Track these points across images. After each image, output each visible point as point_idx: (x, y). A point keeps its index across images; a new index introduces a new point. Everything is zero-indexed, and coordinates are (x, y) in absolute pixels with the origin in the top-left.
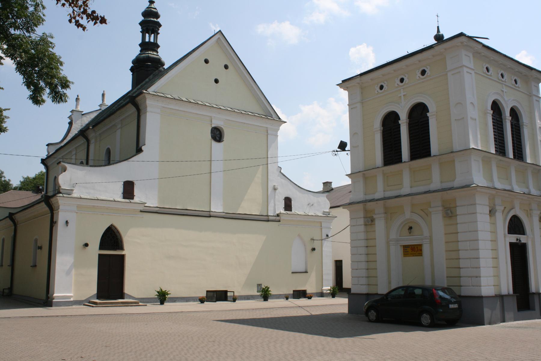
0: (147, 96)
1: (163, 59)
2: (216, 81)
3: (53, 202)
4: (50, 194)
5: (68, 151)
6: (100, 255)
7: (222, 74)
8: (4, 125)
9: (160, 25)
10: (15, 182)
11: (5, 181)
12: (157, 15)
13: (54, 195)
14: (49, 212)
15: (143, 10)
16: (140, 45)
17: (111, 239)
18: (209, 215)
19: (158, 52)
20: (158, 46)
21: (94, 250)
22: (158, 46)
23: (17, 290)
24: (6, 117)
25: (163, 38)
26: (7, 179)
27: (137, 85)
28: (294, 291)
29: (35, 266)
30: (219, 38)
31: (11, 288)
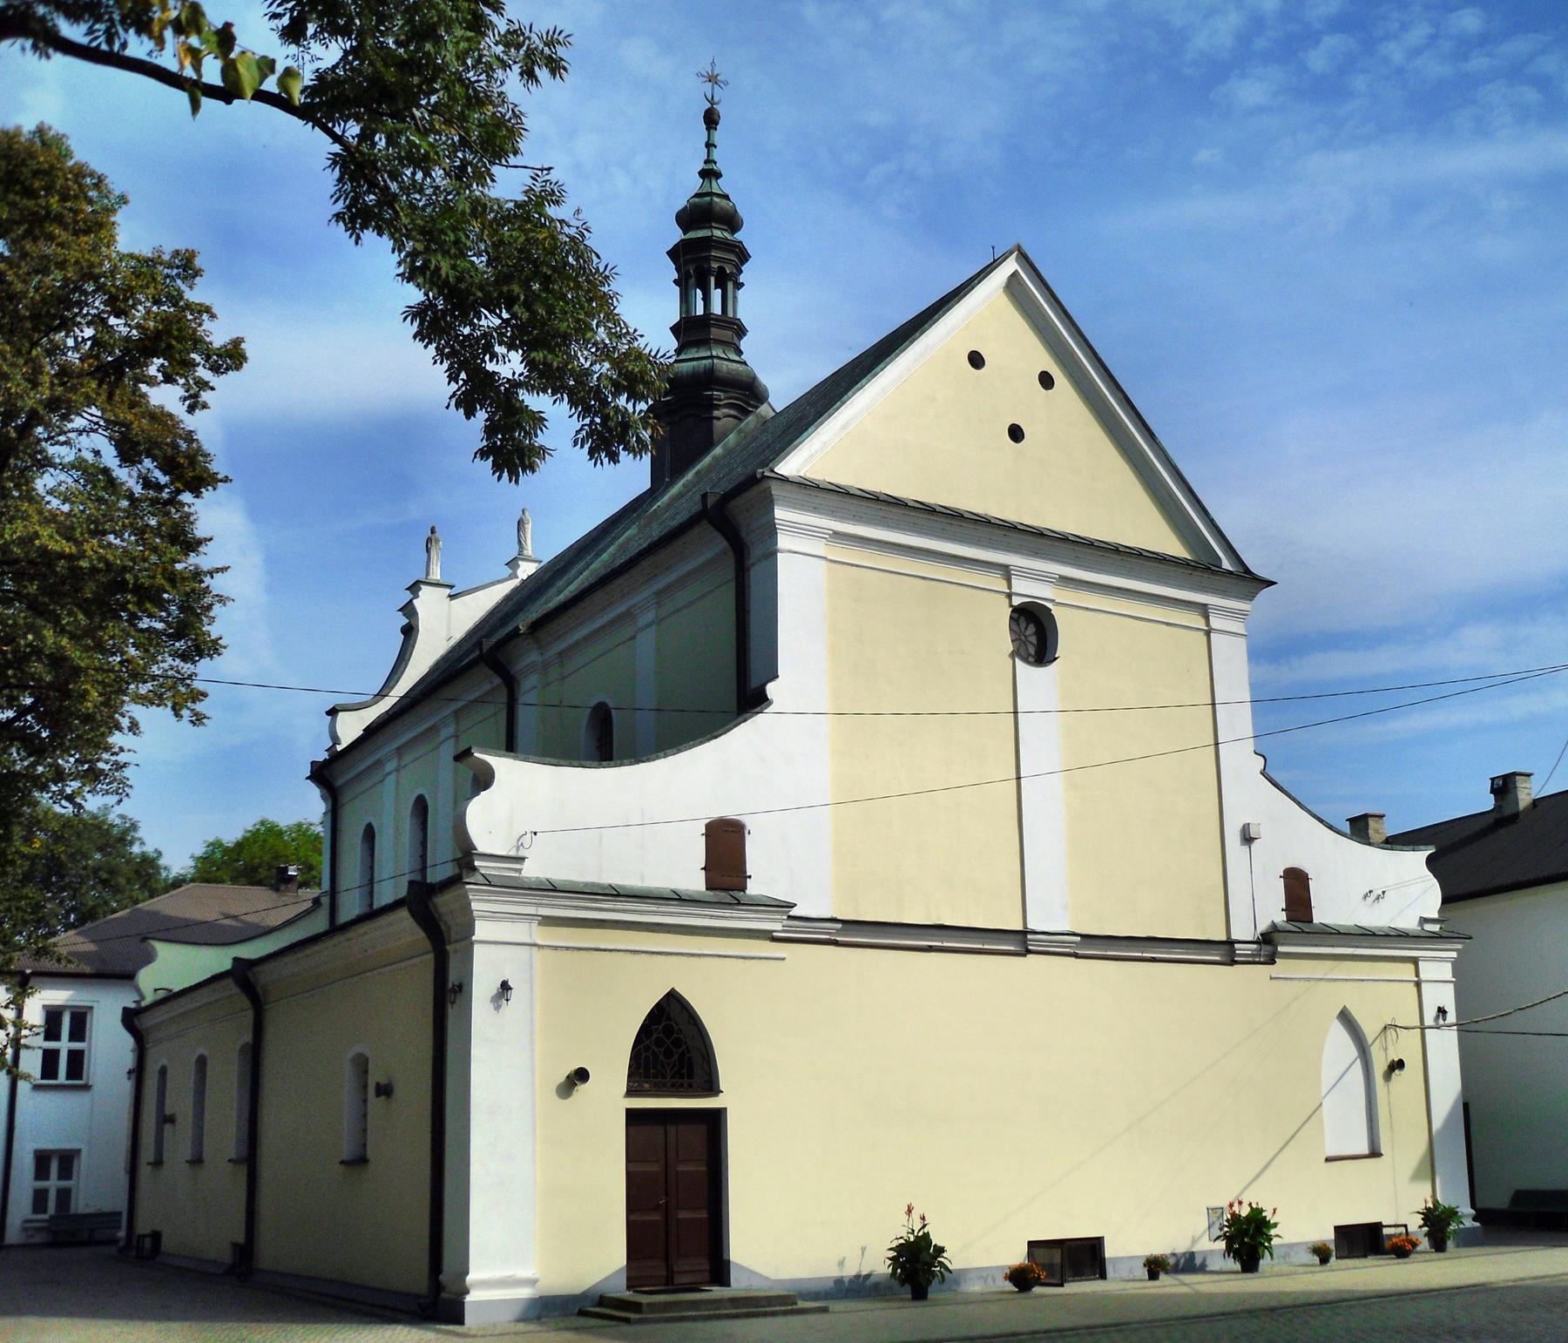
0: (776, 489)
1: (766, 379)
2: (1016, 433)
3: (442, 910)
4: (436, 875)
5: (425, 726)
6: (633, 1116)
7: (1034, 408)
8: (214, 630)
9: (743, 256)
10: (178, 860)
11: (143, 854)
12: (732, 221)
13: (455, 881)
14: (428, 945)
15: (681, 203)
16: (675, 330)
17: (672, 1047)
18: (1021, 942)
19: (740, 352)
20: (741, 331)
21: (610, 1097)
22: (741, 331)
23: (269, 1254)
24: (222, 599)
25: (755, 301)
26: (149, 849)
27: (678, 471)
28: (1339, 1230)
29: (359, 1161)
30: (1015, 275)
31: (245, 1252)
